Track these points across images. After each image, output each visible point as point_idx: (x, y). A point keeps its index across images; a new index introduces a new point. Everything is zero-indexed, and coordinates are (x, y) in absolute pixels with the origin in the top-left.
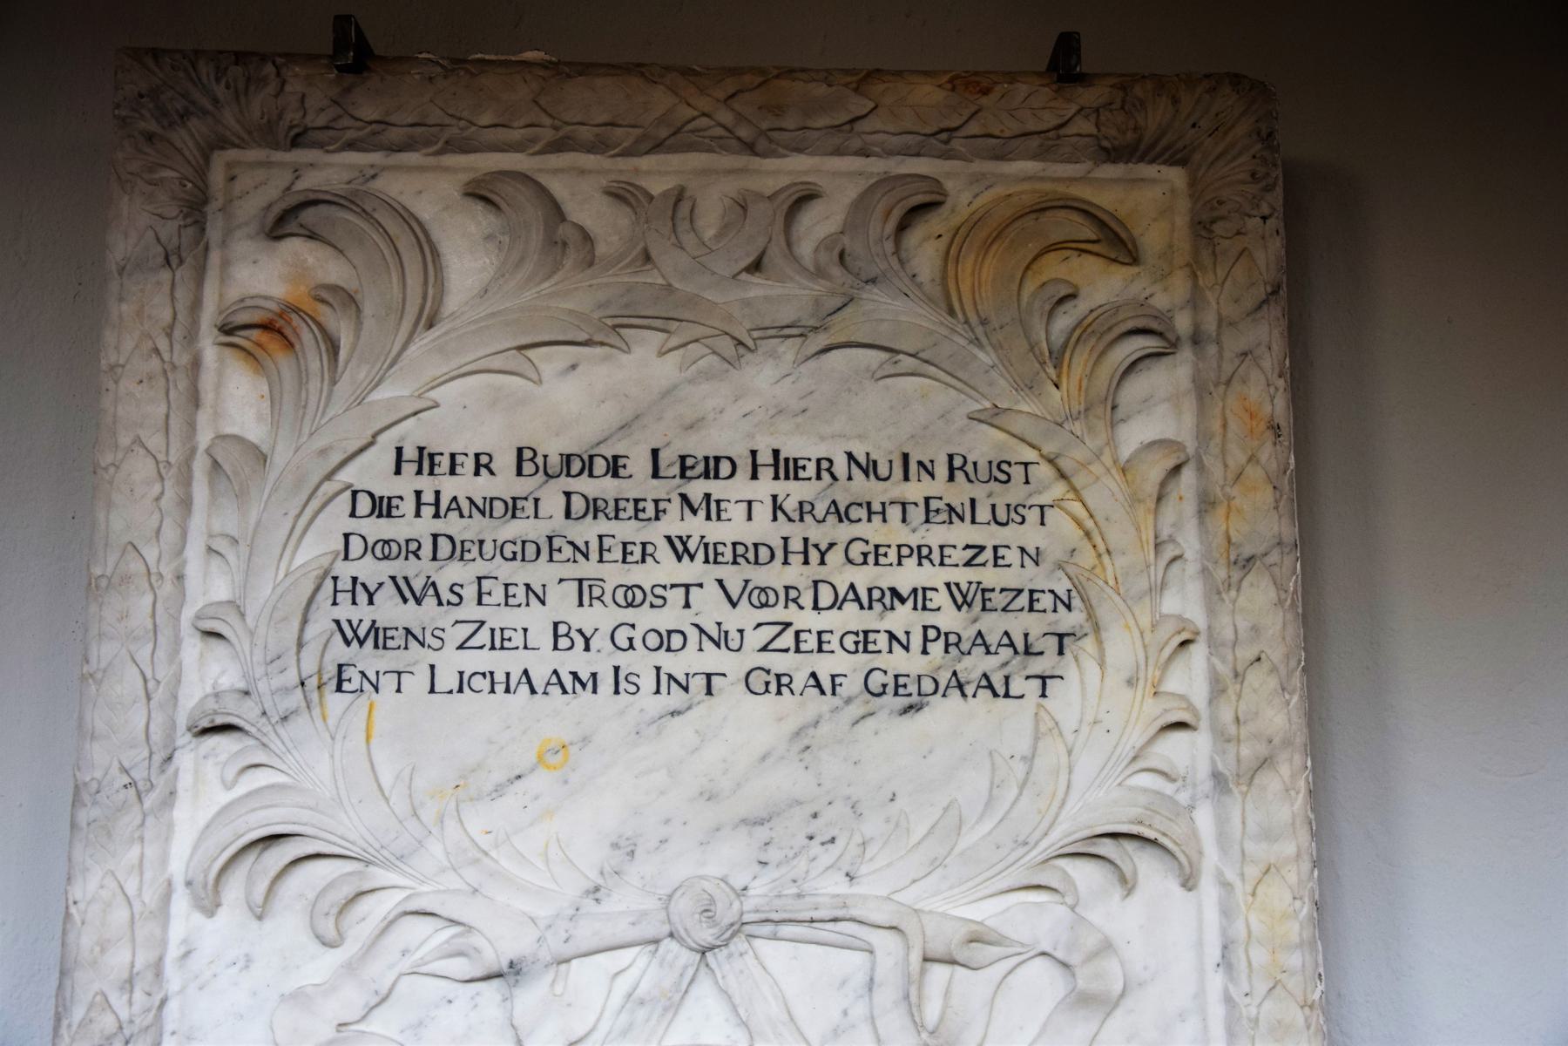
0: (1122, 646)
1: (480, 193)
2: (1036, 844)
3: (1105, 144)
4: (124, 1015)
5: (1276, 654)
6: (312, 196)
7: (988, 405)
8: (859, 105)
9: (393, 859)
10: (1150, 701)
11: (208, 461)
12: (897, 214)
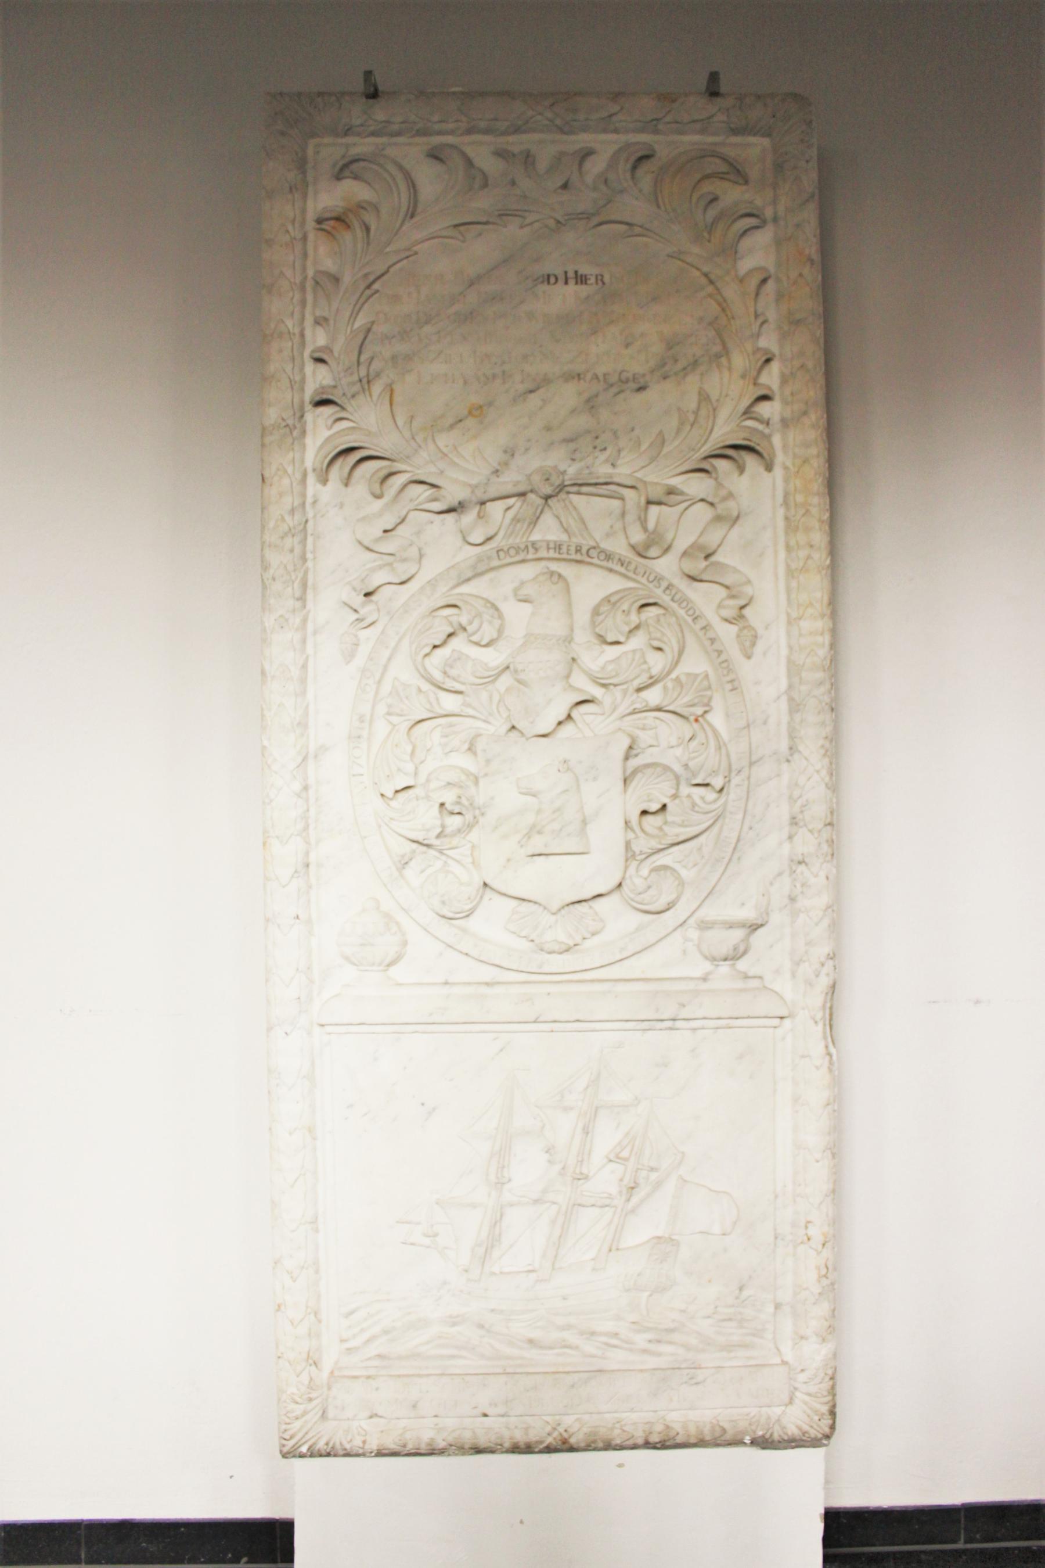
0: (739, 361)
1: (435, 155)
2: (700, 449)
3: (732, 126)
4: (291, 525)
5: (810, 364)
6: (357, 157)
7: (675, 249)
8: (616, 108)
9: (404, 458)
10: (751, 387)
11: (313, 282)
12: (633, 158)
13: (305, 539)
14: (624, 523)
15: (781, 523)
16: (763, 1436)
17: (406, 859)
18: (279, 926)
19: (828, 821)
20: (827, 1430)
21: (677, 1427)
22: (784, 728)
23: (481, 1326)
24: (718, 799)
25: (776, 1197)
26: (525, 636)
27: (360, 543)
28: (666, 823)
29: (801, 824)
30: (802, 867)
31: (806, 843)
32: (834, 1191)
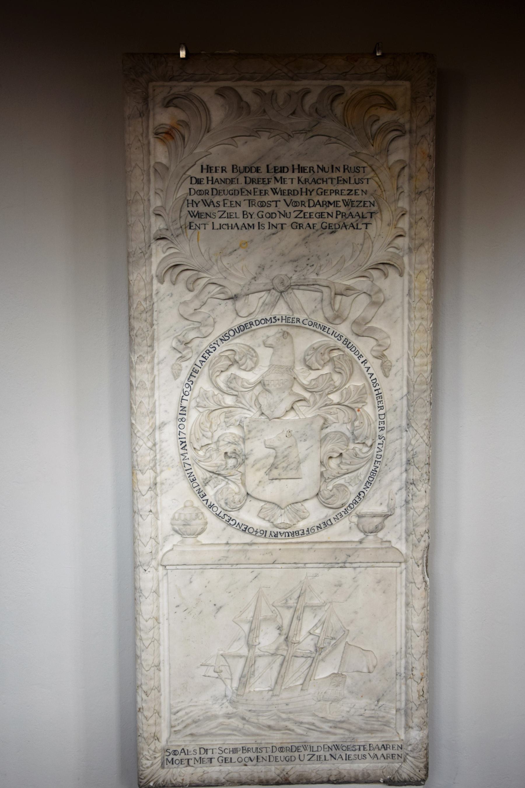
0: (387, 216)
4: (145, 306)
5: (426, 217)
7: (354, 151)
12: (331, 98)
13: (153, 313)
14: (322, 306)
15: (406, 306)
16: (390, 778)
17: (207, 481)
18: (141, 516)
19: (427, 462)
20: (423, 777)
21: (345, 773)
22: (405, 413)
23: (243, 719)
24: (369, 451)
25: (397, 654)
26: (269, 366)
27: (182, 316)
28: (341, 463)
29: (413, 464)
30: (413, 486)
31: (415, 474)
32: (427, 652)
